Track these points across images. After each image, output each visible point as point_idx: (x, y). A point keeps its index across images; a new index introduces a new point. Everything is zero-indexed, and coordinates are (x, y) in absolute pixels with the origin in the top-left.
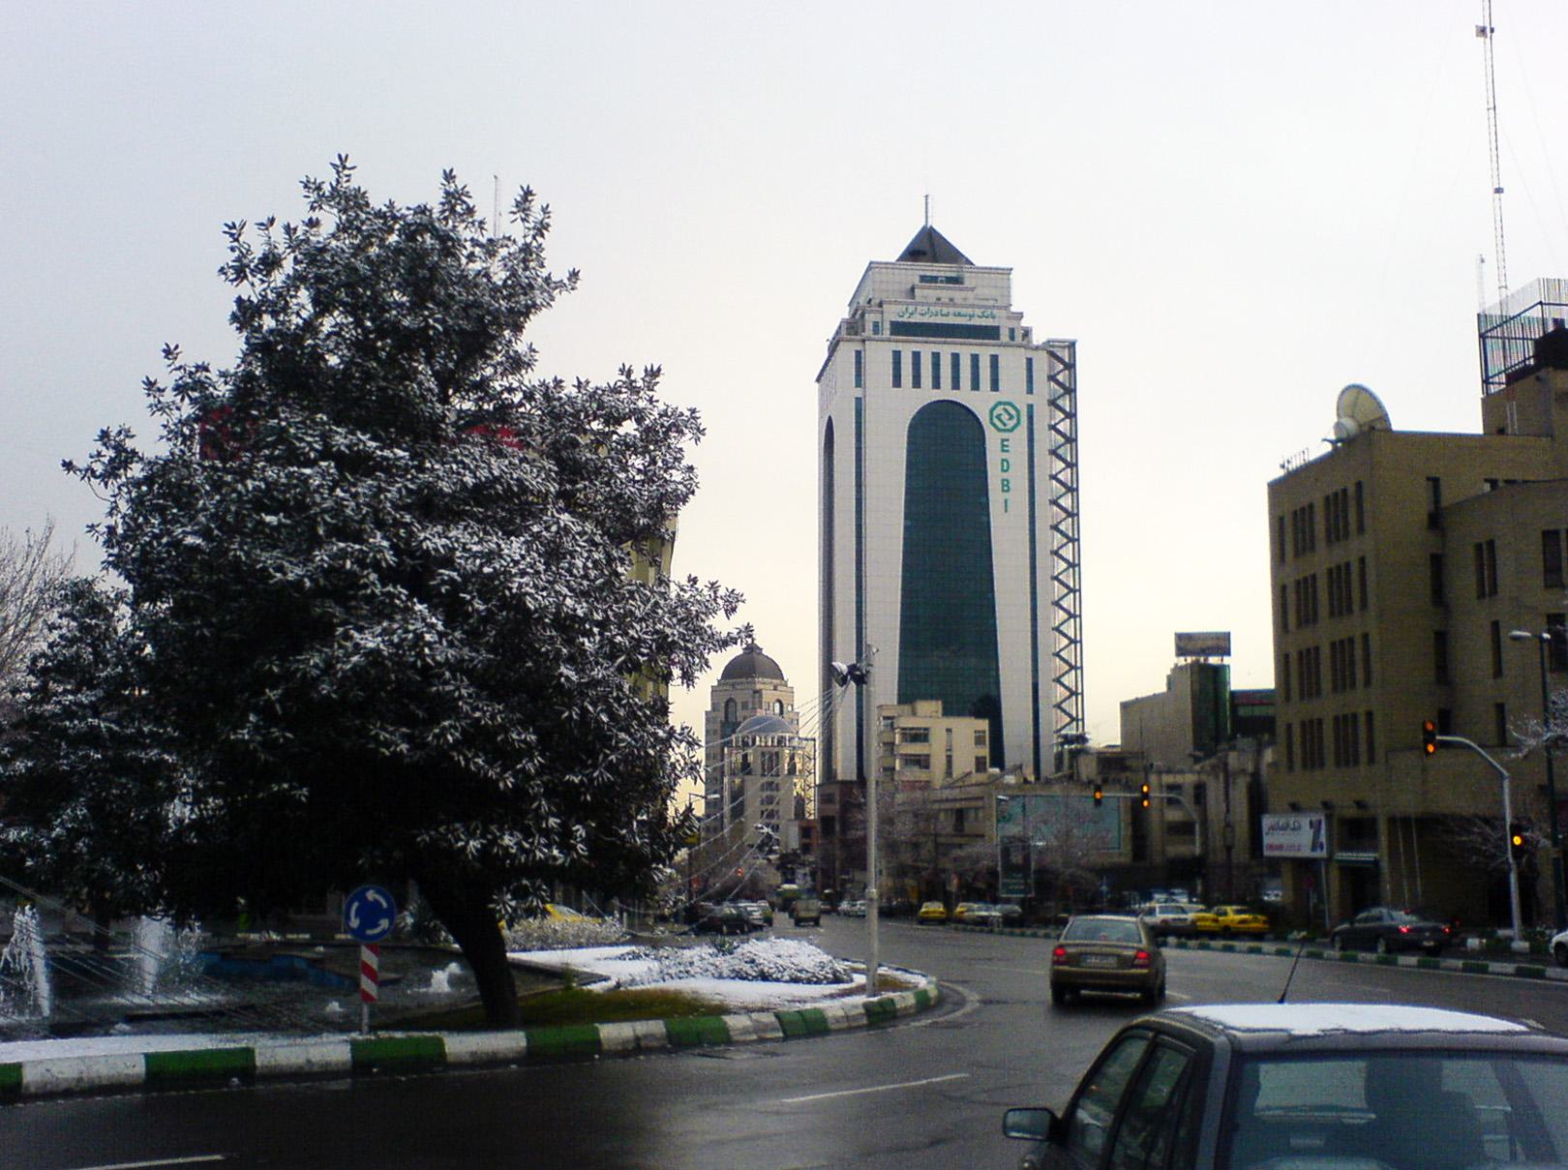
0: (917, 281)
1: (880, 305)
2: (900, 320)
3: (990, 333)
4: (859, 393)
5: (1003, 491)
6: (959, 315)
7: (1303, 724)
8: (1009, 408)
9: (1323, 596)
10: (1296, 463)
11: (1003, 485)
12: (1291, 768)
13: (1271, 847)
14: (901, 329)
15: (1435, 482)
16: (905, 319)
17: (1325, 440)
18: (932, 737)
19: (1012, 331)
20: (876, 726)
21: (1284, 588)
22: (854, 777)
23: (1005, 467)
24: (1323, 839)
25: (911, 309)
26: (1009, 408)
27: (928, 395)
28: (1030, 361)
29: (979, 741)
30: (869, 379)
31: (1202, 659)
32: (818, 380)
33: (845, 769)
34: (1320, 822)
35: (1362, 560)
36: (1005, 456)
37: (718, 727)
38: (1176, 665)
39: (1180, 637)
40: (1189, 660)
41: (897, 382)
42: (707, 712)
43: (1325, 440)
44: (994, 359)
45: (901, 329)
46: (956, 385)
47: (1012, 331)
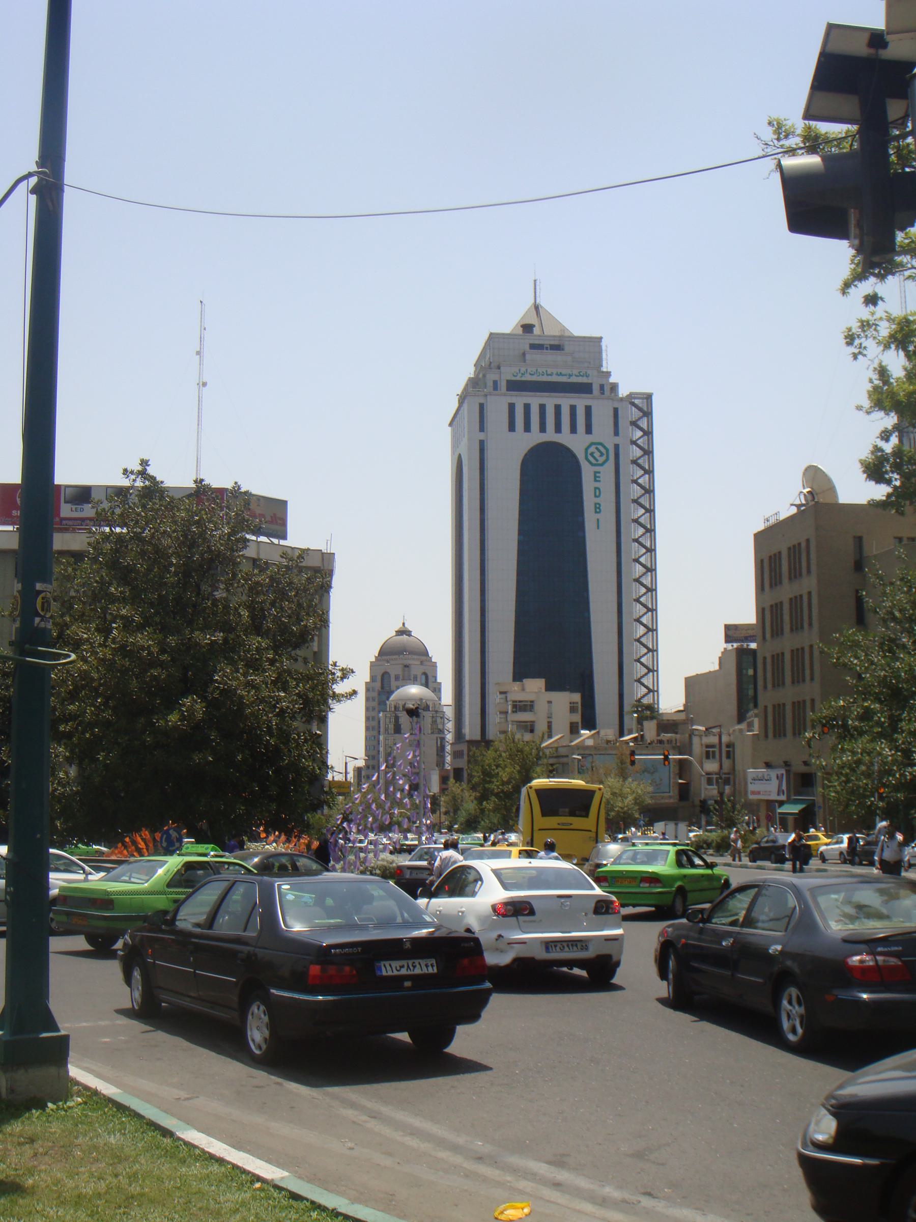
0: (527, 347)
1: (499, 368)
2: (514, 379)
3: (584, 389)
4: (482, 436)
5: (596, 512)
6: (561, 374)
7: (774, 706)
8: (600, 447)
9: (787, 618)
10: (772, 521)
11: (599, 508)
12: (766, 736)
13: (753, 793)
14: (515, 386)
15: (859, 540)
16: (518, 378)
17: (792, 505)
18: (536, 707)
19: (602, 387)
20: (494, 698)
21: (763, 610)
22: (478, 738)
23: (597, 492)
24: (784, 787)
25: (523, 370)
26: (600, 447)
27: (536, 437)
28: (616, 411)
29: (573, 710)
30: (490, 424)
31: (745, 645)
32: (451, 424)
33: (471, 731)
34: (782, 775)
35: (810, 593)
36: (597, 485)
37: (375, 694)
38: (725, 649)
39: (728, 628)
40: (735, 645)
41: (512, 427)
42: (366, 683)
43: (792, 505)
44: (588, 410)
45: (515, 386)
46: (558, 429)
47: (602, 387)
